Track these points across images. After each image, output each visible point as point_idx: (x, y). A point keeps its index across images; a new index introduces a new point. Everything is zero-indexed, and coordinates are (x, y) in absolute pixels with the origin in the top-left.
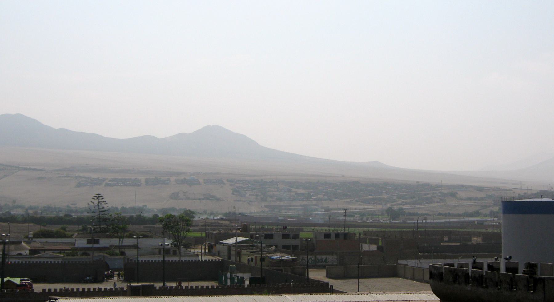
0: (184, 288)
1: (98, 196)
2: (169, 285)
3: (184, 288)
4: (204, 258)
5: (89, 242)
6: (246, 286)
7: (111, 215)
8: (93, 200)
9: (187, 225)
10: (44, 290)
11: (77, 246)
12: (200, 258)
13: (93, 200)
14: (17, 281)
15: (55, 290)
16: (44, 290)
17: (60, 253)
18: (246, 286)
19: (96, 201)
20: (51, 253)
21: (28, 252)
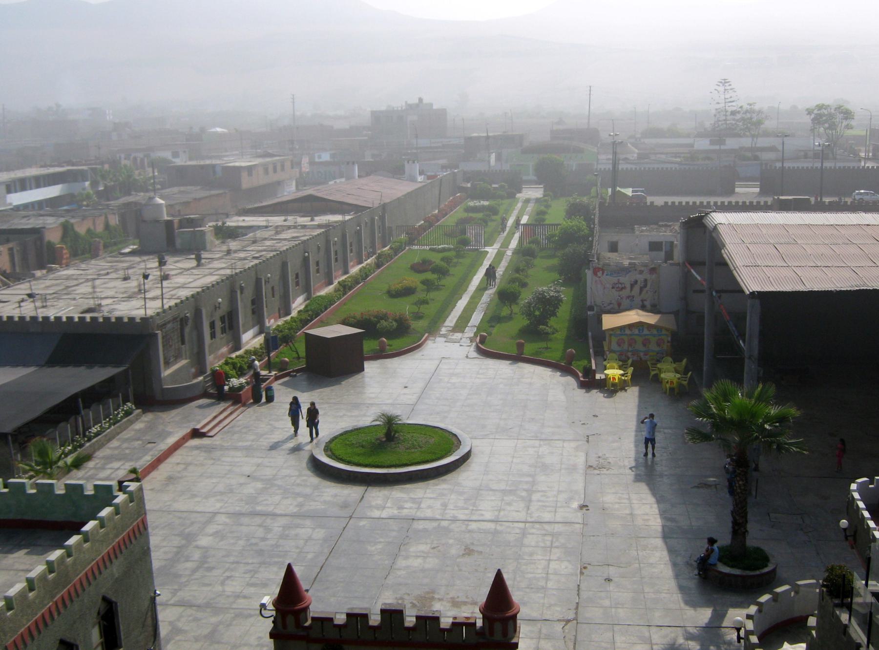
0: (648, 204)
1: (725, 82)
2: (827, 200)
3: (648, 204)
4: (870, 165)
5: (712, 143)
6: (685, 361)
7: (741, 107)
8: (717, 87)
9: (846, 119)
10: (666, 203)
11: (696, 147)
12: (863, 164)
13: (717, 87)
14: (629, 192)
15: (730, 203)
16: (666, 203)
17: (676, 157)
18: (685, 361)
19: (721, 89)
20: (663, 156)
21: (636, 155)
